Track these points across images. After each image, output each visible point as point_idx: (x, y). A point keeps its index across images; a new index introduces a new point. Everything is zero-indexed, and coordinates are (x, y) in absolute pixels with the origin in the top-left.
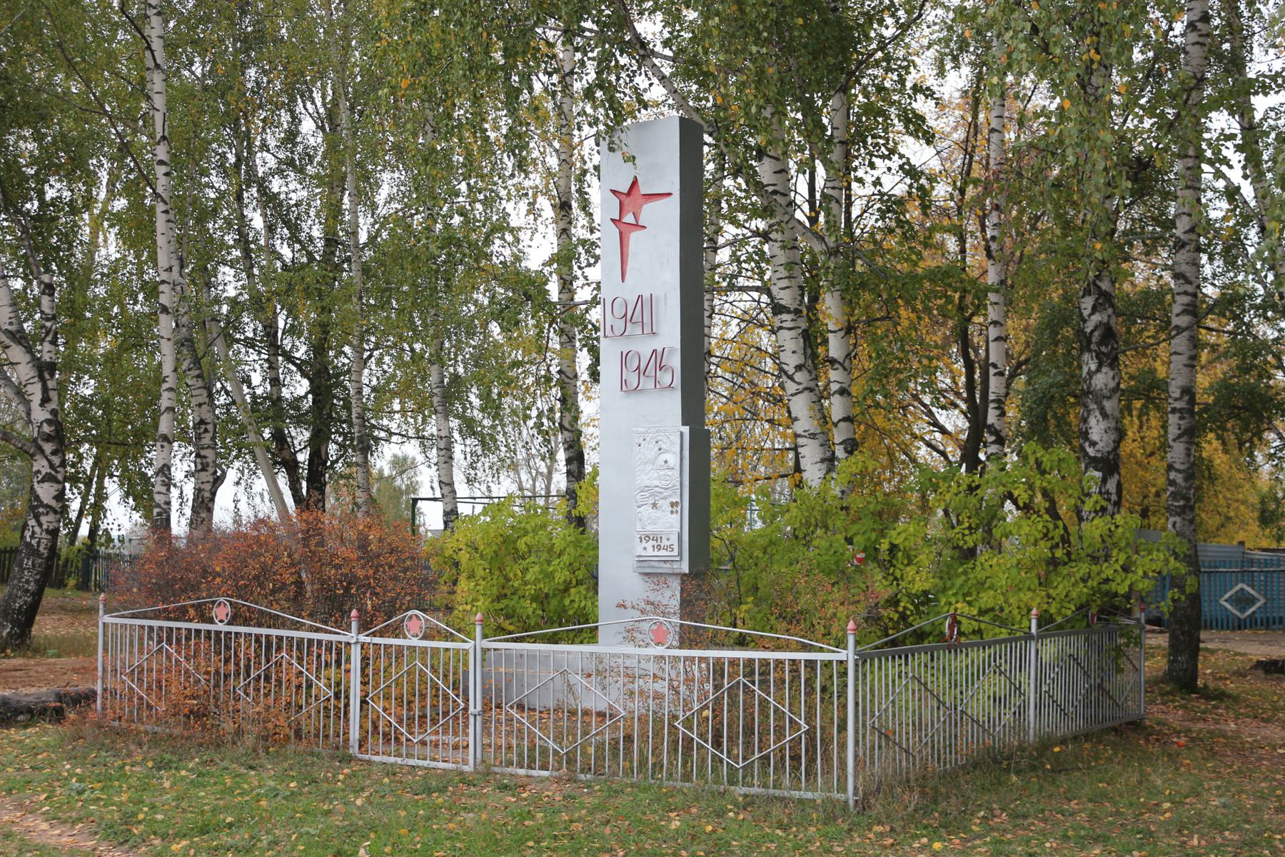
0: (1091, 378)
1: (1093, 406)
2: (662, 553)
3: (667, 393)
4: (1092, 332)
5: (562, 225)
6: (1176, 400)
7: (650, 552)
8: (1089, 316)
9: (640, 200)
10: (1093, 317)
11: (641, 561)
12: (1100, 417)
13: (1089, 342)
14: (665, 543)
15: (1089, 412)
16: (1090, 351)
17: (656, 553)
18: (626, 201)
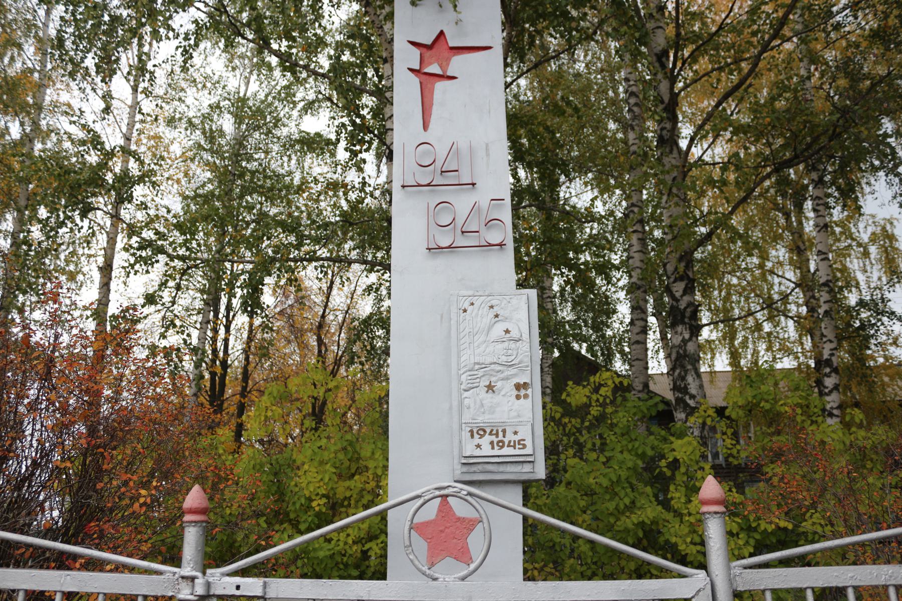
0: (685, 345)
1: (689, 367)
2: (506, 451)
3: (494, 254)
4: (685, 308)
5: (106, 280)
6: (639, 391)
7: (486, 450)
8: (682, 296)
9: (446, 54)
10: (684, 298)
11: (468, 463)
12: (695, 376)
13: (683, 316)
14: (510, 437)
15: (686, 371)
16: (684, 323)
17: (496, 452)
18: (428, 54)
